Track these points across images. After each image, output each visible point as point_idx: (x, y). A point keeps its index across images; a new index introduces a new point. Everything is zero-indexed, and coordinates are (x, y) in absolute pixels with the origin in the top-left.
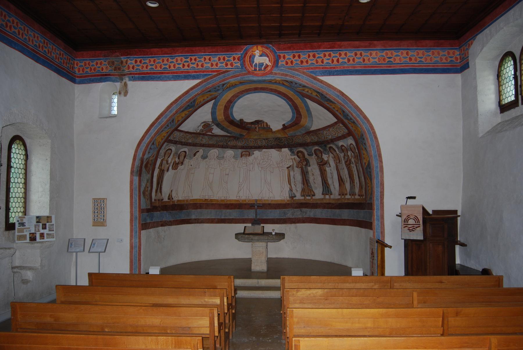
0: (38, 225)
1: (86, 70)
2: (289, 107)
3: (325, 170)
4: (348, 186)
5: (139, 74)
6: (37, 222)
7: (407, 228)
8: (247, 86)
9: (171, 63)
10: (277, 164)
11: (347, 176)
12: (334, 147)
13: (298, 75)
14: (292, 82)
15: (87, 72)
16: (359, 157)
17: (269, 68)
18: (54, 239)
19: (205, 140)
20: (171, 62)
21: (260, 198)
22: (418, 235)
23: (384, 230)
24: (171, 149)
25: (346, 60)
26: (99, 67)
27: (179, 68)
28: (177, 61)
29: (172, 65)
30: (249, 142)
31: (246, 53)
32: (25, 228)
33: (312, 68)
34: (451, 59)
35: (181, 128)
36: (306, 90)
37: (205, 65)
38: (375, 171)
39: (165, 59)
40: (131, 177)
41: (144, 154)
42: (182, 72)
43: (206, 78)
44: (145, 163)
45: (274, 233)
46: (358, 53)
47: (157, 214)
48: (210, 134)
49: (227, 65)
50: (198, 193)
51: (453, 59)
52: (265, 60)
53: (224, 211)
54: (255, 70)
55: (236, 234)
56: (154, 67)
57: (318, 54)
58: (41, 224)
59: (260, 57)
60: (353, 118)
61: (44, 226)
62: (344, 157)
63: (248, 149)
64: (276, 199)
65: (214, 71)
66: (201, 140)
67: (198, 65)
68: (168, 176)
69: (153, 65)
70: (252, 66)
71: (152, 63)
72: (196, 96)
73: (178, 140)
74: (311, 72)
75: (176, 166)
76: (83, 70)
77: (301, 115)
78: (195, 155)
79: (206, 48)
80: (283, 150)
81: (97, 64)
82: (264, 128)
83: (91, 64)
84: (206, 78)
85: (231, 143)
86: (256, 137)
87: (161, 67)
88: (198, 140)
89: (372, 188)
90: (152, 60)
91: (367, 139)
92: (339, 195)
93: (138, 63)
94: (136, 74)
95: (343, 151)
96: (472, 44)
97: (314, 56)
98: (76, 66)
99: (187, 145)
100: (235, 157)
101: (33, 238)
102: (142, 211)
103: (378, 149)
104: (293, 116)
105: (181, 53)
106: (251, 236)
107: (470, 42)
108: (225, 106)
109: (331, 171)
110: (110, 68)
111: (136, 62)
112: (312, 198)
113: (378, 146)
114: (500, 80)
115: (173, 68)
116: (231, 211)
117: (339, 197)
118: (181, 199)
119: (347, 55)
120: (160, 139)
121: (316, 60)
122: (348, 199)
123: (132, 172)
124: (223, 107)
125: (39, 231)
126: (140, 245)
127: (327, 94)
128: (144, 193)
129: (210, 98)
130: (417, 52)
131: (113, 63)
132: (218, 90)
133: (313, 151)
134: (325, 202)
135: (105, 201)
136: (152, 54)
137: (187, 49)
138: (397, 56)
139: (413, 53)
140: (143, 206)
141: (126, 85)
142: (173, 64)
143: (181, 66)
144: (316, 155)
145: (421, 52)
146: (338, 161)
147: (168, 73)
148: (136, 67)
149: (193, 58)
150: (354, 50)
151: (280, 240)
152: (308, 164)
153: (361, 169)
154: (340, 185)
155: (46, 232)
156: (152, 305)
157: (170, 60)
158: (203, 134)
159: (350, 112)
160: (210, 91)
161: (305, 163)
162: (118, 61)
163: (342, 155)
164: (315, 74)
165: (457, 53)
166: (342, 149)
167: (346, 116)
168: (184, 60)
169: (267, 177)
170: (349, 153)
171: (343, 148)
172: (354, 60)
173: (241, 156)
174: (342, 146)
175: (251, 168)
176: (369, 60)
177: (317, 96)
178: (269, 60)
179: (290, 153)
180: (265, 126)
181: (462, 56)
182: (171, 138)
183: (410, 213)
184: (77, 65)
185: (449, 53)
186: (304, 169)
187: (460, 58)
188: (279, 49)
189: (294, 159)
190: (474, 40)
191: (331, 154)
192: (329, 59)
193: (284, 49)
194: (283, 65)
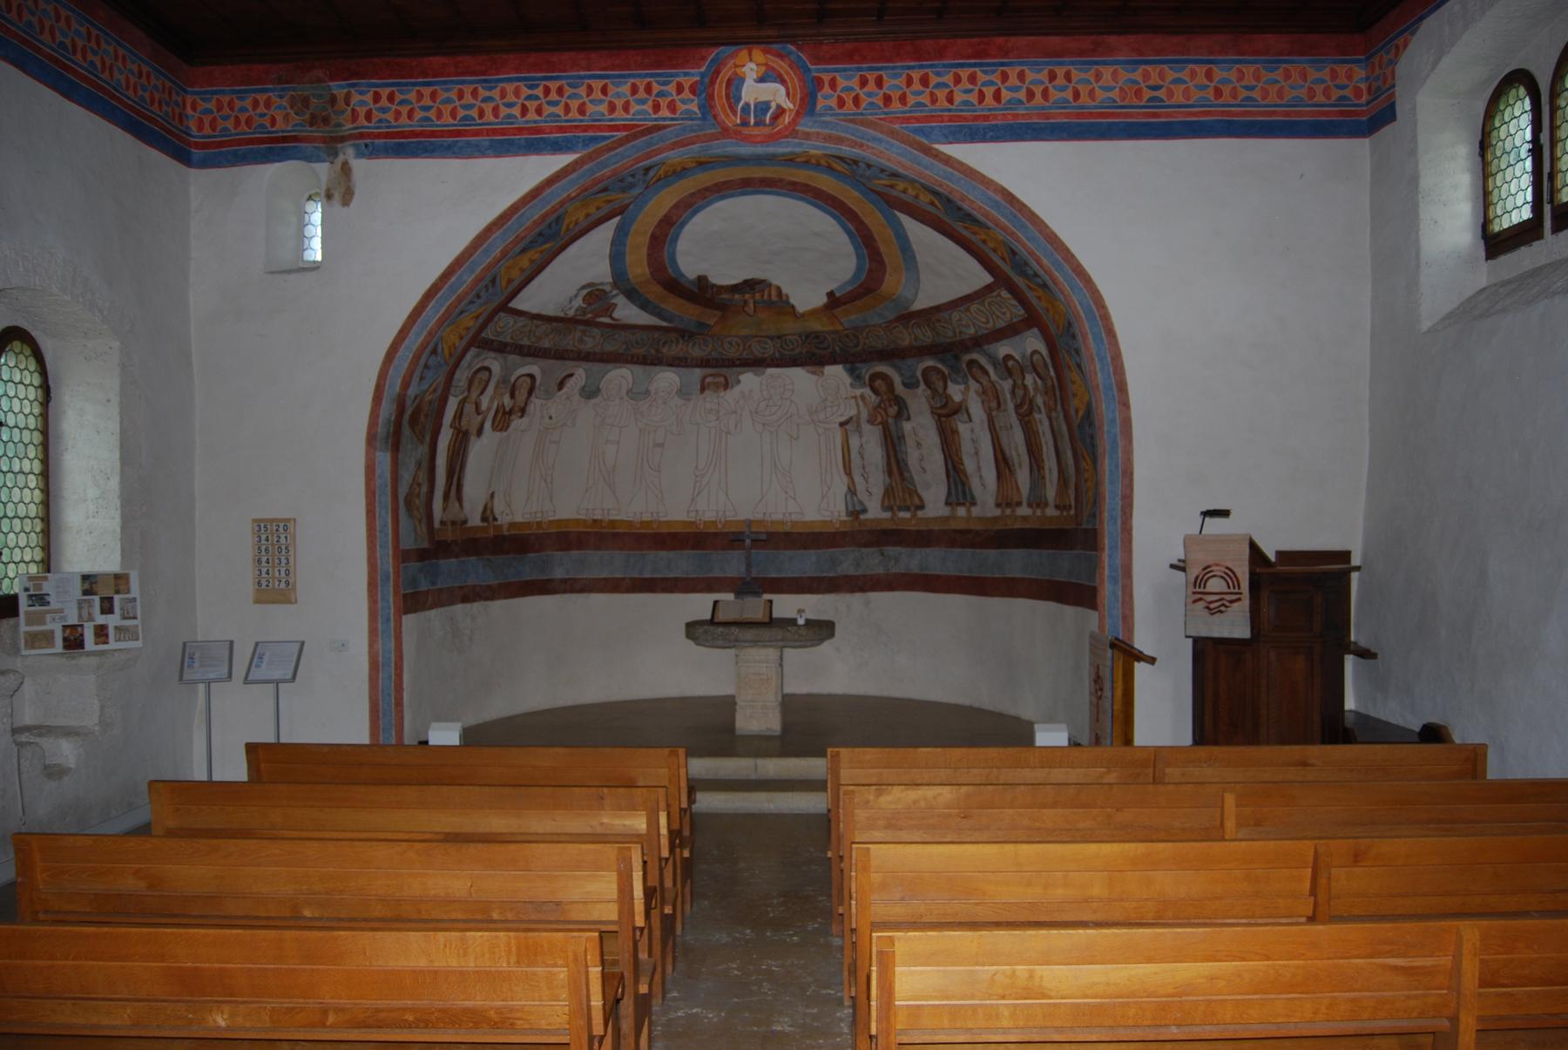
1: (221, 124)
3: (955, 432)
4: (1023, 477)
6: (85, 593)
7: (1201, 604)
11: (1023, 449)
12: (983, 361)
13: (875, 139)
14: (856, 162)
15: (226, 129)
16: (1059, 391)
17: (787, 119)
18: (139, 644)
21: (759, 516)
22: (1235, 625)
23: (1132, 609)
24: (488, 369)
25: (1022, 95)
27: (509, 116)
28: (503, 95)
29: (488, 108)
30: (726, 346)
31: (718, 72)
33: (918, 120)
34: (1341, 93)
36: (901, 186)
37: (591, 108)
39: (468, 89)
41: (406, 384)
42: (520, 130)
44: (409, 411)
45: (801, 622)
47: (447, 564)
48: (606, 320)
49: (657, 107)
50: (571, 502)
52: (775, 94)
54: (745, 123)
55: (689, 625)
56: (432, 114)
57: (938, 74)
58: (97, 599)
59: (759, 83)
60: (1041, 272)
61: (107, 605)
62: (1013, 393)
63: (720, 368)
66: (581, 341)
67: (567, 109)
68: (481, 451)
70: (735, 113)
71: (427, 101)
72: (562, 203)
73: (508, 340)
74: (916, 131)
75: (503, 419)
77: (882, 263)
78: (561, 385)
80: (829, 369)
82: (769, 304)
83: (238, 104)
85: (671, 350)
86: (745, 332)
87: (453, 114)
88: (571, 341)
89: (1097, 485)
90: (427, 91)
91: (1085, 336)
92: (998, 505)
93: (384, 102)
94: (378, 136)
97: (925, 81)
98: (189, 111)
100: (683, 393)
101: (74, 642)
102: (403, 556)
104: (859, 269)
105: (517, 70)
106: (735, 630)
107: (1400, 41)
108: (654, 237)
109: (974, 434)
111: (377, 97)
112: (914, 516)
115: (492, 119)
116: (672, 554)
117: (998, 512)
118: (519, 519)
119: (1026, 79)
121: (932, 94)
122: (1025, 518)
123: (371, 439)
124: (645, 240)
127: (963, 198)
129: (606, 209)
130: (1240, 71)
131: (306, 102)
132: (632, 186)
133: (919, 374)
135: (291, 525)
139: (1225, 74)
140: (408, 543)
141: (346, 170)
142: (491, 105)
143: (516, 111)
144: (928, 384)
145: (1249, 70)
146: (994, 405)
147: (477, 133)
148: (377, 115)
149: (554, 85)
150: (1047, 64)
151: (821, 641)
152: (902, 412)
153: (1064, 428)
154: (999, 476)
155: (112, 621)
157: (483, 93)
158: (588, 323)
159: (1031, 253)
160: (605, 190)
161: (893, 410)
163: (1006, 385)
164: (927, 136)
165: (1360, 73)
166: (1007, 367)
167: (1021, 267)
168: (526, 92)
169: (779, 452)
170: (1029, 380)
171: (1010, 363)
172: (1045, 94)
173: (703, 389)
174: (1008, 357)
176: (1092, 93)
177: (932, 204)
178: (788, 94)
179: (848, 380)
182: (488, 333)
184: (194, 109)
185: (1334, 75)
186: (893, 428)
188: (818, 60)
189: (862, 397)
190: (1413, 33)
191: (974, 385)
192: (970, 91)
193: (833, 59)
194: (831, 108)
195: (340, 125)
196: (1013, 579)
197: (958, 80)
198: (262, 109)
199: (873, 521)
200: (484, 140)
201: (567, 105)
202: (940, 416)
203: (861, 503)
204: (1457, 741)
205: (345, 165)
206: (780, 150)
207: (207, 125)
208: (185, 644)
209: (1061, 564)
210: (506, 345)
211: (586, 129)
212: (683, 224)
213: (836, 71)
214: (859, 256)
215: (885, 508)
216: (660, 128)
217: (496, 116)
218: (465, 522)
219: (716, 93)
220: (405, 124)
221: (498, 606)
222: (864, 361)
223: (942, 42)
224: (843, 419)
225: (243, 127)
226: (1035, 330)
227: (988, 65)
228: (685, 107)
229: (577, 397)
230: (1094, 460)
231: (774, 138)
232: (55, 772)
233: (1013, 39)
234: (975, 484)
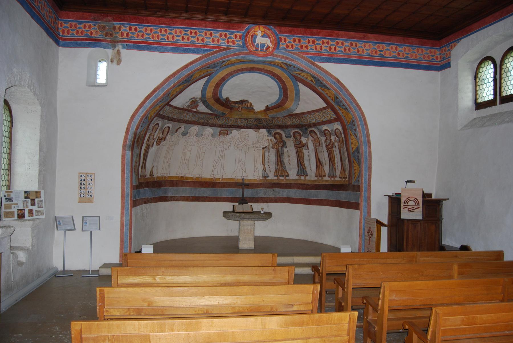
0: (27, 201)
1: (71, 32)
2: (278, 89)
3: (302, 152)
4: (327, 168)
5: (134, 42)
6: (26, 198)
7: (406, 209)
8: (245, 66)
9: (169, 34)
10: (253, 144)
12: (316, 131)
13: (297, 59)
14: (290, 66)
15: (73, 34)
16: (345, 142)
17: (270, 50)
18: (44, 217)
19: (188, 117)
21: (233, 177)
24: (158, 124)
25: (342, 49)
26: (87, 31)
27: (178, 40)
28: (176, 32)
29: (170, 36)
31: (248, 33)
32: (13, 204)
33: (311, 54)
34: (432, 57)
35: (172, 103)
36: (303, 74)
37: (206, 40)
40: (123, 151)
42: (181, 45)
43: (206, 53)
44: (137, 138)
45: (262, 212)
46: (354, 43)
47: (142, 190)
48: (195, 110)
49: (228, 42)
50: (175, 171)
51: (434, 58)
52: (267, 41)
53: (199, 189)
54: (257, 50)
57: (317, 40)
58: (29, 200)
59: (262, 37)
60: (346, 105)
61: (33, 202)
62: (326, 141)
63: (226, 128)
64: (249, 178)
65: (215, 48)
67: (198, 39)
69: (150, 34)
70: (254, 46)
71: (148, 32)
72: (195, 71)
73: (166, 115)
74: (311, 57)
75: (160, 140)
76: (68, 32)
78: (177, 131)
80: (261, 130)
81: (85, 27)
82: (247, 108)
83: (78, 26)
84: (206, 53)
86: (237, 117)
88: (182, 117)
90: (149, 28)
91: (358, 125)
92: (316, 176)
93: (133, 31)
94: (131, 42)
95: (325, 135)
96: (455, 46)
97: (313, 42)
98: (59, 26)
99: (172, 121)
100: (213, 135)
101: (21, 216)
103: (367, 135)
104: (279, 99)
105: (181, 25)
106: (243, 215)
107: (453, 44)
108: (217, 84)
109: (309, 155)
110: (101, 33)
111: (131, 29)
112: (285, 178)
113: (368, 132)
114: (478, 80)
116: (205, 189)
117: (316, 178)
118: (160, 176)
119: (344, 44)
121: (315, 46)
122: (327, 181)
123: (124, 146)
125: (27, 207)
126: (131, 223)
127: (324, 80)
128: (135, 169)
129: (205, 74)
131: (104, 27)
132: (216, 67)
133: (292, 134)
134: (299, 182)
135: (93, 176)
136: (148, 23)
138: (387, 50)
139: (401, 49)
140: (134, 183)
141: (118, 52)
142: (172, 35)
143: (180, 38)
144: (294, 137)
146: (318, 144)
147: (166, 45)
148: (130, 35)
149: (194, 31)
152: (284, 144)
153: (346, 153)
154: (317, 167)
155: (35, 208)
156: (219, 284)
158: (189, 111)
159: (344, 99)
160: (208, 67)
161: (281, 145)
162: (110, 26)
164: (314, 59)
165: (438, 52)
166: (324, 133)
167: (339, 103)
168: (184, 32)
169: (242, 156)
170: (333, 138)
171: (326, 132)
172: (349, 50)
173: (220, 135)
174: (326, 130)
176: (363, 51)
177: (312, 81)
179: (267, 134)
180: (249, 106)
181: (443, 56)
182: (161, 113)
183: (410, 196)
184: (61, 26)
185: (431, 52)
186: (280, 150)
187: (441, 57)
188: (281, 32)
190: (458, 42)
192: (327, 47)
193: (285, 32)
196: (321, 200)
197: (323, 43)
198: (87, 29)
199: (271, 180)
200: (169, 47)
201: (198, 38)
202: (297, 147)
204: (473, 250)
205: (118, 51)
206: (268, 60)
208: (83, 217)
210: (164, 116)
211: (204, 47)
213: (286, 36)
214: (280, 95)
215: (275, 176)
217: (173, 39)
218: (146, 176)
222: (273, 128)
223: (319, 30)
224: (264, 147)
225: (80, 34)
226: (339, 122)
227: (333, 39)
228: (237, 43)
229: (180, 135)
230: (359, 164)
231: (266, 56)
232: (20, 264)
234: (308, 170)
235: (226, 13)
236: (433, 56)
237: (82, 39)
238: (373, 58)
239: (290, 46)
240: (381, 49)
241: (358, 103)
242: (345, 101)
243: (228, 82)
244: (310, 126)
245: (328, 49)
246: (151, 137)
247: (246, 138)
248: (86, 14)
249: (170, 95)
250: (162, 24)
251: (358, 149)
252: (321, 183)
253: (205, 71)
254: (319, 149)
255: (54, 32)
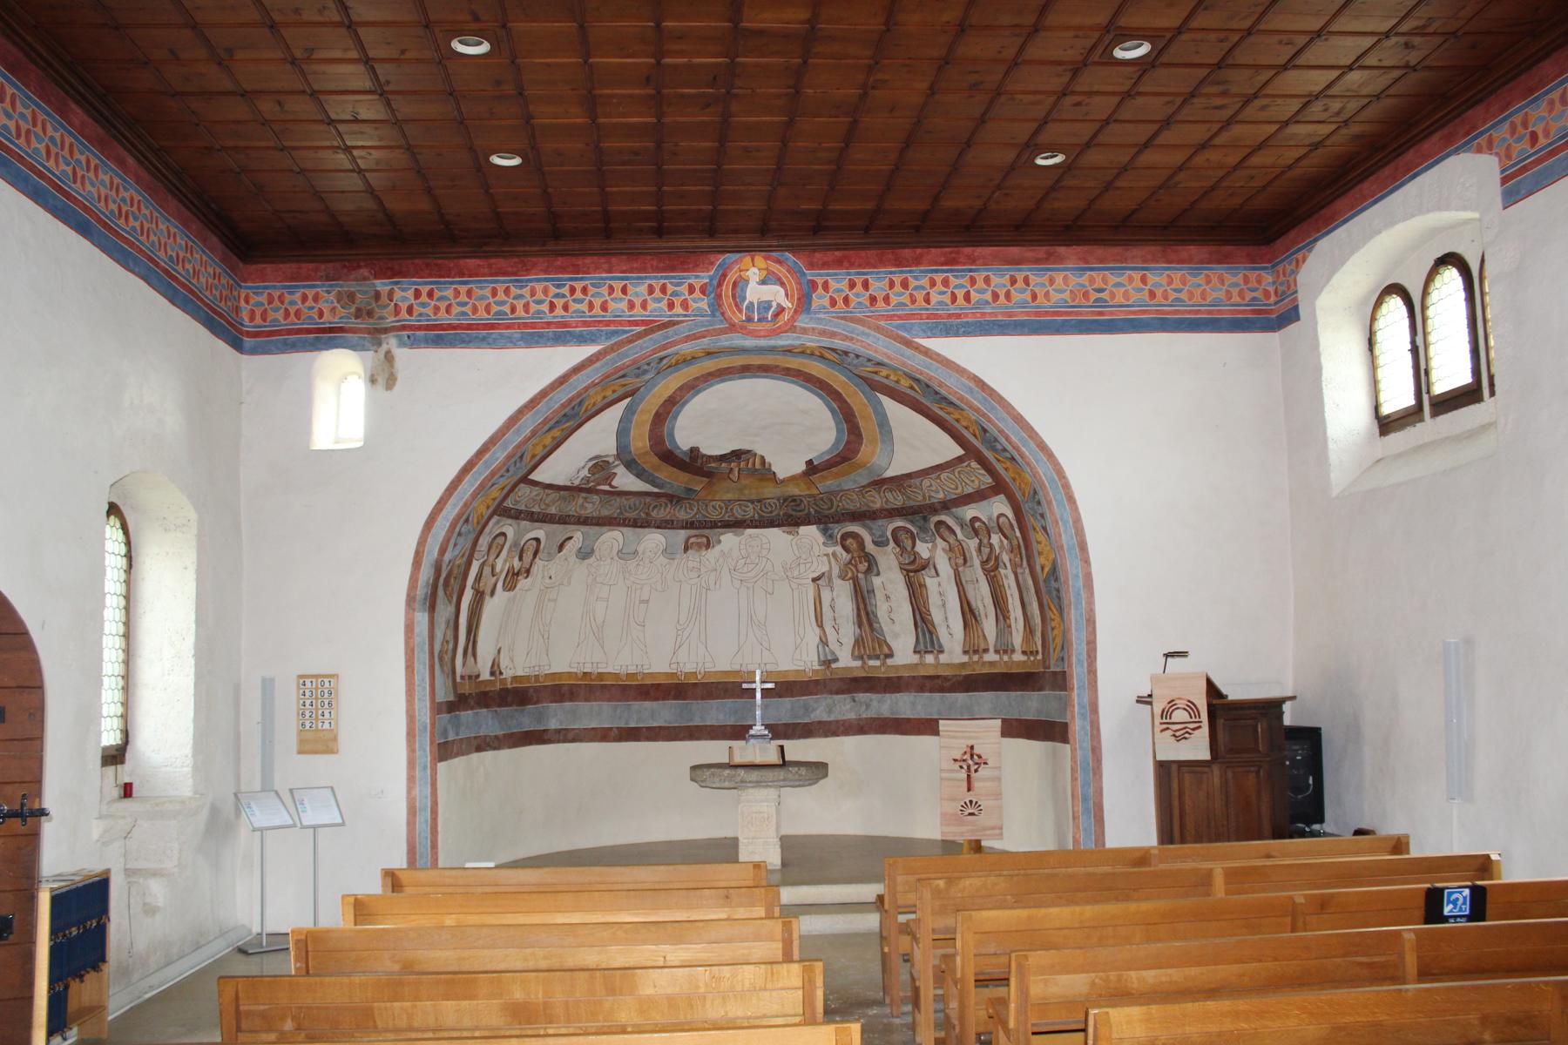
1: (271, 315)
3: (923, 586)
4: (989, 626)
5: (428, 328)
7: (1169, 733)
11: (989, 601)
13: (863, 334)
14: (846, 353)
15: (276, 320)
16: (1025, 550)
19: (591, 507)
20: (518, 297)
21: (737, 668)
22: (1197, 748)
23: (1099, 742)
24: (504, 534)
25: (988, 296)
27: (539, 312)
28: (533, 294)
29: (519, 305)
30: (710, 509)
31: (724, 275)
33: (900, 317)
35: (536, 476)
37: (612, 306)
38: (1073, 584)
39: (501, 288)
41: (443, 551)
42: (549, 324)
44: (444, 575)
46: (1020, 276)
47: (467, 715)
48: (607, 488)
49: (671, 305)
50: (565, 657)
53: (636, 705)
54: (749, 319)
55: (694, 768)
56: (468, 309)
57: (916, 278)
59: (761, 283)
60: (1009, 447)
63: (704, 529)
65: (636, 323)
68: (493, 607)
70: (740, 311)
72: (587, 389)
74: (898, 327)
75: (512, 578)
77: (859, 436)
79: (614, 260)
80: (803, 529)
82: (753, 472)
83: (288, 298)
85: (659, 514)
86: (729, 496)
87: (488, 310)
89: (1065, 633)
90: (463, 289)
92: (965, 652)
93: (424, 298)
94: (419, 328)
95: (976, 533)
97: (905, 285)
98: (243, 303)
100: (668, 552)
102: (438, 708)
104: (838, 441)
105: (546, 272)
106: (742, 772)
107: (1299, 255)
108: (657, 415)
109: (941, 590)
110: (341, 311)
111: (417, 294)
112: (884, 664)
115: (523, 314)
116: (655, 704)
117: (965, 659)
119: (993, 280)
120: (483, 509)
122: (992, 663)
123: (410, 599)
124: (649, 417)
126: (435, 803)
127: (941, 384)
128: (441, 659)
129: (620, 392)
131: (352, 297)
132: (646, 372)
134: (923, 673)
136: (462, 275)
137: (559, 261)
138: (1118, 285)
139: (1157, 279)
141: (389, 357)
142: (522, 302)
143: (545, 307)
145: (1177, 276)
146: (961, 561)
147: (508, 327)
148: (417, 309)
149: (579, 285)
151: (816, 781)
152: (872, 566)
153: (1030, 582)
158: (589, 491)
159: (1001, 432)
161: (863, 566)
163: (972, 544)
164: (908, 331)
165: (1268, 278)
166: (973, 527)
167: (992, 443)
168: (553, 290)
169: (759, 607)
171: (977, 524)
173: (686, 549)
174: (975, 519)
175: (712, 582)
176: (1047, 294)
177: (912, 388)
179: (821, 539)
180: (758, 466)
181: (1281, 289)
182: (509, 503)
184: (247, 302)
186: (863, 582)
188: (812, 266)
189: (834, 554)
190: (1310, 251)
193: (825, 265)
195: (382, 318)
198: (310, 303)
203: (833, 653)
207: (258, 317)
209: (1031, 705)
210: (521, 511)
211: (608, 323)
212: (685, 404)
216: (673, 323)
217: (527, 311)
219: (723, 293)
220: (444, 319)
221: (505, 754)
223: (919, 251)
228: (695, 305)
230: (1061, 610)
233: (979, 250)
235: (659, 232)
236: (1253, 290)
237: (299, 331)
238: (1077, 314)
239: (840, 302)
240: (1099, 284)
241: (1042, 442)
242: (1007, 438)
243: (688, 407)
244: (934, 509)
245: (947, 299)
246: (487, 570)
247: (764, 552)
248: (307, 267)
249: (527, 457)
250: (496, 275)
251: (1054, 569)
252: (979, 670)
253: (620, 386)
254: (966, 574)
255: (228, 322)
